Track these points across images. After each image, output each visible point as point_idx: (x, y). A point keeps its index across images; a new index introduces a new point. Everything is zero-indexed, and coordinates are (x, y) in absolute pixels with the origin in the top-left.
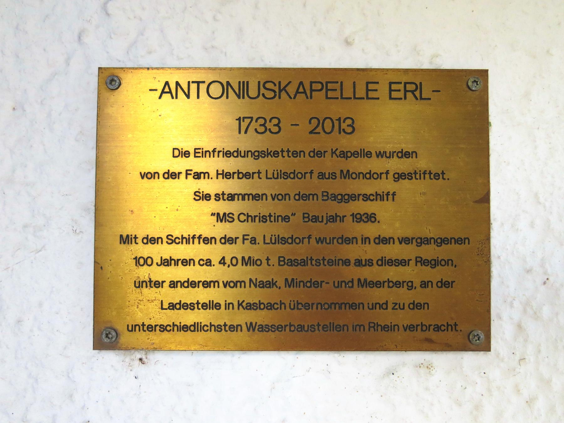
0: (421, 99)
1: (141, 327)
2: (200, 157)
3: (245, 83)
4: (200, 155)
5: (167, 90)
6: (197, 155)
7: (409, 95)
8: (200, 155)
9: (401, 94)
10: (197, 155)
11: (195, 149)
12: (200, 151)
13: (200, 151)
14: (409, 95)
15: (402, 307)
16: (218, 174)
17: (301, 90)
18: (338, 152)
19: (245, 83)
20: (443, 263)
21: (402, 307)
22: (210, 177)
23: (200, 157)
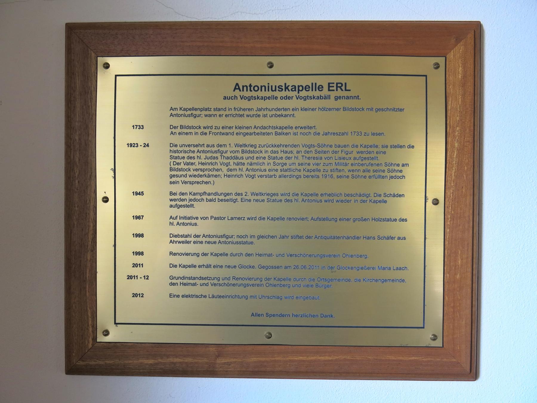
0: (346, 90)
1: (249, 88)
2: (172, 297)
3: (273, 99)
4: (172, 296)
5: (312, 219)
6: (171, 296)
7: (339, 89)
8: (172, 296)
9: (335, 88)
10: (171, 296)
11: (170, 294)
12: (172, 295)
13: (172, 295)
14: (339, 89)
15: (219, 128)
16: (180, 284)
17: (237, 87)
18: (182, 109)
19: (273, 99)
20: (212, 236)
21: (219, 128)
22: (211, 183)
23: (172, 297)
